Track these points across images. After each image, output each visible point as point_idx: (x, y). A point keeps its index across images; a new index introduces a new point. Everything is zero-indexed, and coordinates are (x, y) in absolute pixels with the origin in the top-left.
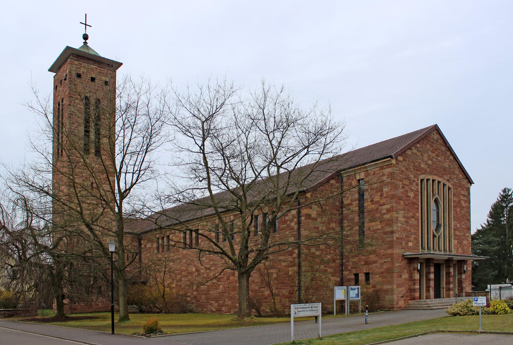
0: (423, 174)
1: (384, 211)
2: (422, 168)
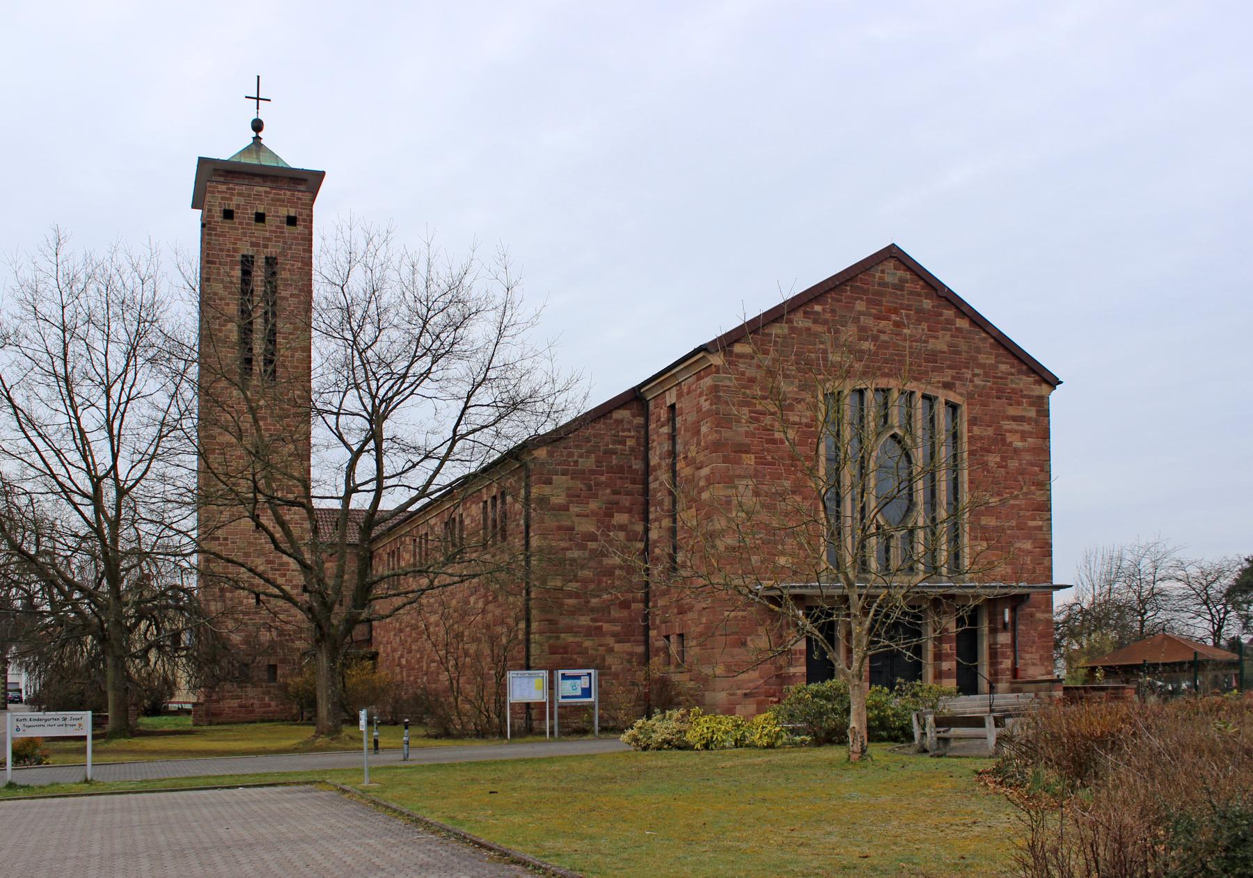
1: (702, 483)
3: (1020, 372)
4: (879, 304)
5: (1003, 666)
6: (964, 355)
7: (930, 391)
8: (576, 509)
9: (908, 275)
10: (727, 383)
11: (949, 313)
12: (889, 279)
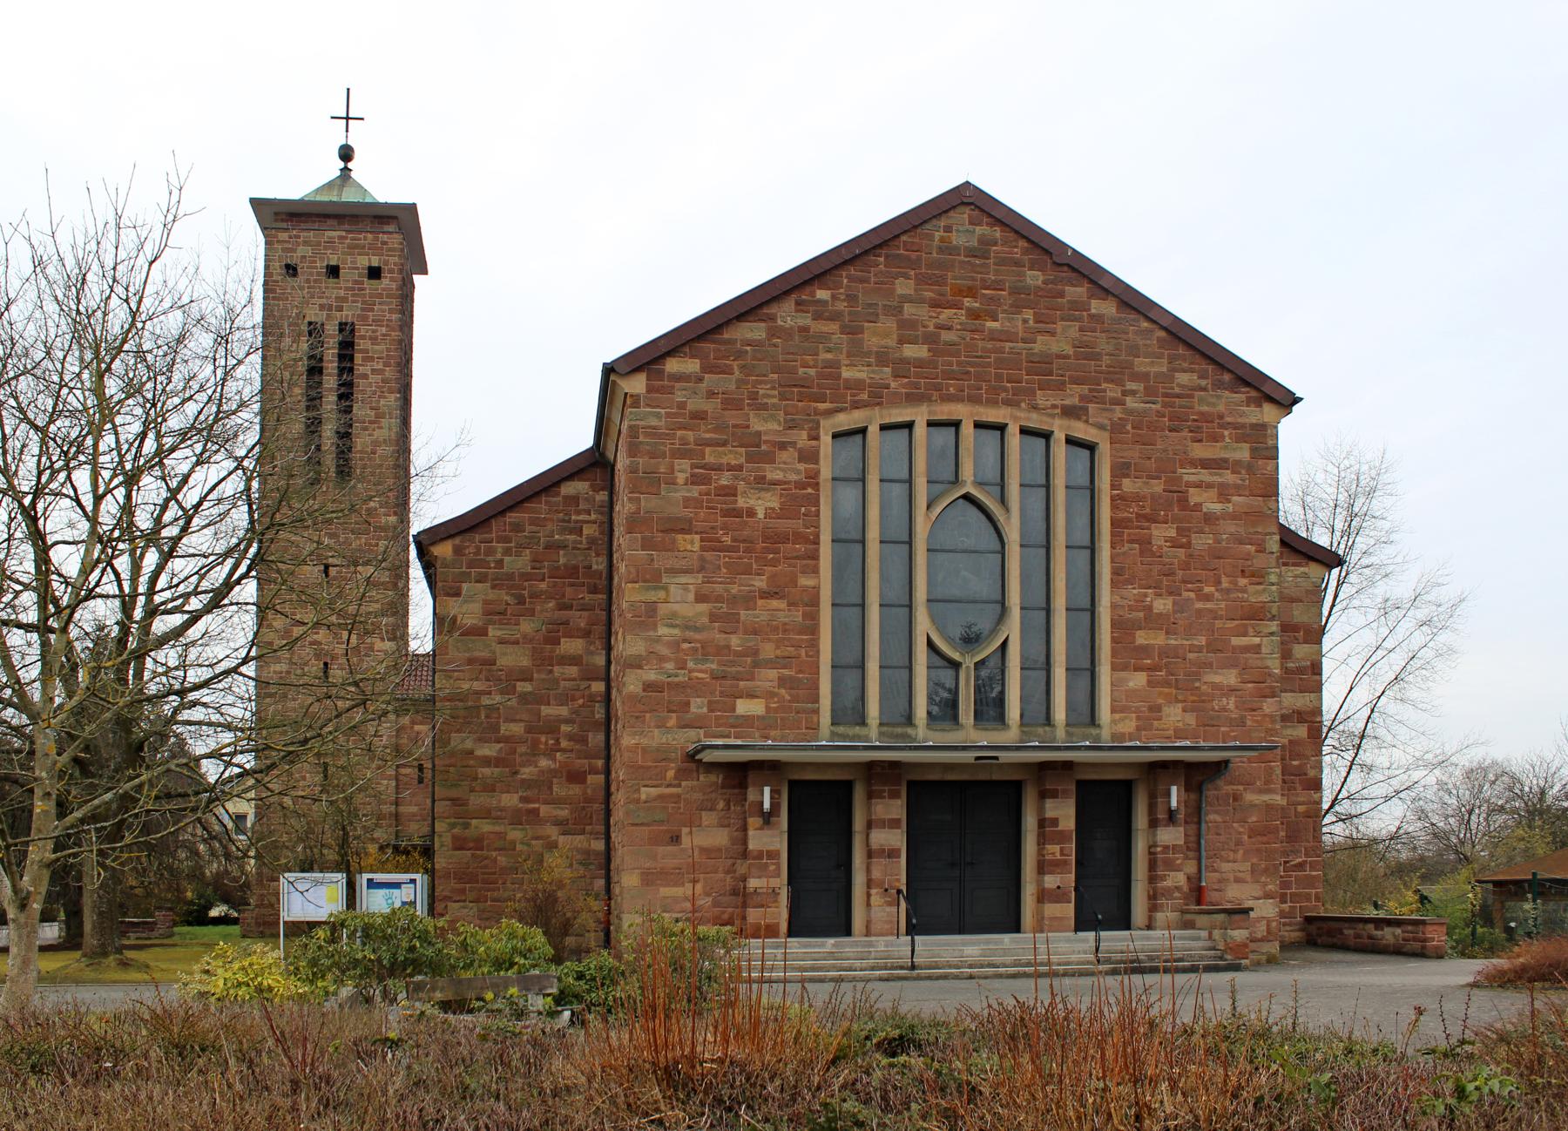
0: (856, 406)
2: (857, 385)
3: (1219, 385)
4: (940, 281)
5: (1168, 883)
6: (1106, 360)
7: (1035, 421)
8: (499, 633)
9: (997, 233)
10: (654, 422)
11: (1078, 291)
12: (958, 239)
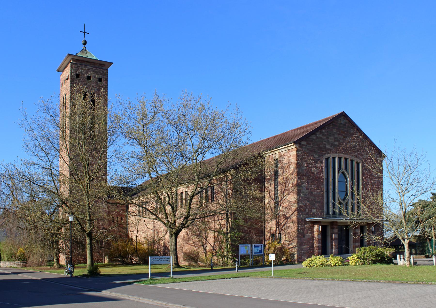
2: (328, 149)
9: (347, 121)
